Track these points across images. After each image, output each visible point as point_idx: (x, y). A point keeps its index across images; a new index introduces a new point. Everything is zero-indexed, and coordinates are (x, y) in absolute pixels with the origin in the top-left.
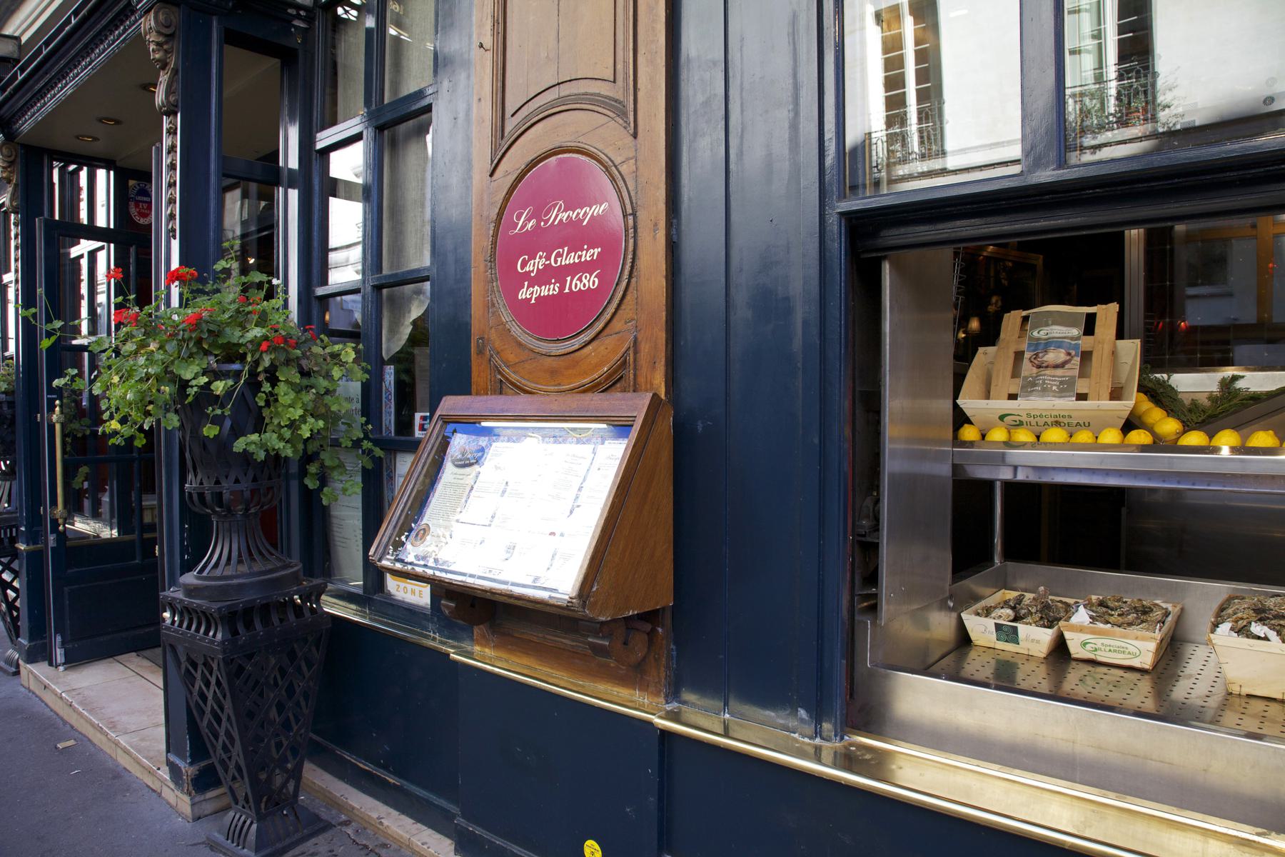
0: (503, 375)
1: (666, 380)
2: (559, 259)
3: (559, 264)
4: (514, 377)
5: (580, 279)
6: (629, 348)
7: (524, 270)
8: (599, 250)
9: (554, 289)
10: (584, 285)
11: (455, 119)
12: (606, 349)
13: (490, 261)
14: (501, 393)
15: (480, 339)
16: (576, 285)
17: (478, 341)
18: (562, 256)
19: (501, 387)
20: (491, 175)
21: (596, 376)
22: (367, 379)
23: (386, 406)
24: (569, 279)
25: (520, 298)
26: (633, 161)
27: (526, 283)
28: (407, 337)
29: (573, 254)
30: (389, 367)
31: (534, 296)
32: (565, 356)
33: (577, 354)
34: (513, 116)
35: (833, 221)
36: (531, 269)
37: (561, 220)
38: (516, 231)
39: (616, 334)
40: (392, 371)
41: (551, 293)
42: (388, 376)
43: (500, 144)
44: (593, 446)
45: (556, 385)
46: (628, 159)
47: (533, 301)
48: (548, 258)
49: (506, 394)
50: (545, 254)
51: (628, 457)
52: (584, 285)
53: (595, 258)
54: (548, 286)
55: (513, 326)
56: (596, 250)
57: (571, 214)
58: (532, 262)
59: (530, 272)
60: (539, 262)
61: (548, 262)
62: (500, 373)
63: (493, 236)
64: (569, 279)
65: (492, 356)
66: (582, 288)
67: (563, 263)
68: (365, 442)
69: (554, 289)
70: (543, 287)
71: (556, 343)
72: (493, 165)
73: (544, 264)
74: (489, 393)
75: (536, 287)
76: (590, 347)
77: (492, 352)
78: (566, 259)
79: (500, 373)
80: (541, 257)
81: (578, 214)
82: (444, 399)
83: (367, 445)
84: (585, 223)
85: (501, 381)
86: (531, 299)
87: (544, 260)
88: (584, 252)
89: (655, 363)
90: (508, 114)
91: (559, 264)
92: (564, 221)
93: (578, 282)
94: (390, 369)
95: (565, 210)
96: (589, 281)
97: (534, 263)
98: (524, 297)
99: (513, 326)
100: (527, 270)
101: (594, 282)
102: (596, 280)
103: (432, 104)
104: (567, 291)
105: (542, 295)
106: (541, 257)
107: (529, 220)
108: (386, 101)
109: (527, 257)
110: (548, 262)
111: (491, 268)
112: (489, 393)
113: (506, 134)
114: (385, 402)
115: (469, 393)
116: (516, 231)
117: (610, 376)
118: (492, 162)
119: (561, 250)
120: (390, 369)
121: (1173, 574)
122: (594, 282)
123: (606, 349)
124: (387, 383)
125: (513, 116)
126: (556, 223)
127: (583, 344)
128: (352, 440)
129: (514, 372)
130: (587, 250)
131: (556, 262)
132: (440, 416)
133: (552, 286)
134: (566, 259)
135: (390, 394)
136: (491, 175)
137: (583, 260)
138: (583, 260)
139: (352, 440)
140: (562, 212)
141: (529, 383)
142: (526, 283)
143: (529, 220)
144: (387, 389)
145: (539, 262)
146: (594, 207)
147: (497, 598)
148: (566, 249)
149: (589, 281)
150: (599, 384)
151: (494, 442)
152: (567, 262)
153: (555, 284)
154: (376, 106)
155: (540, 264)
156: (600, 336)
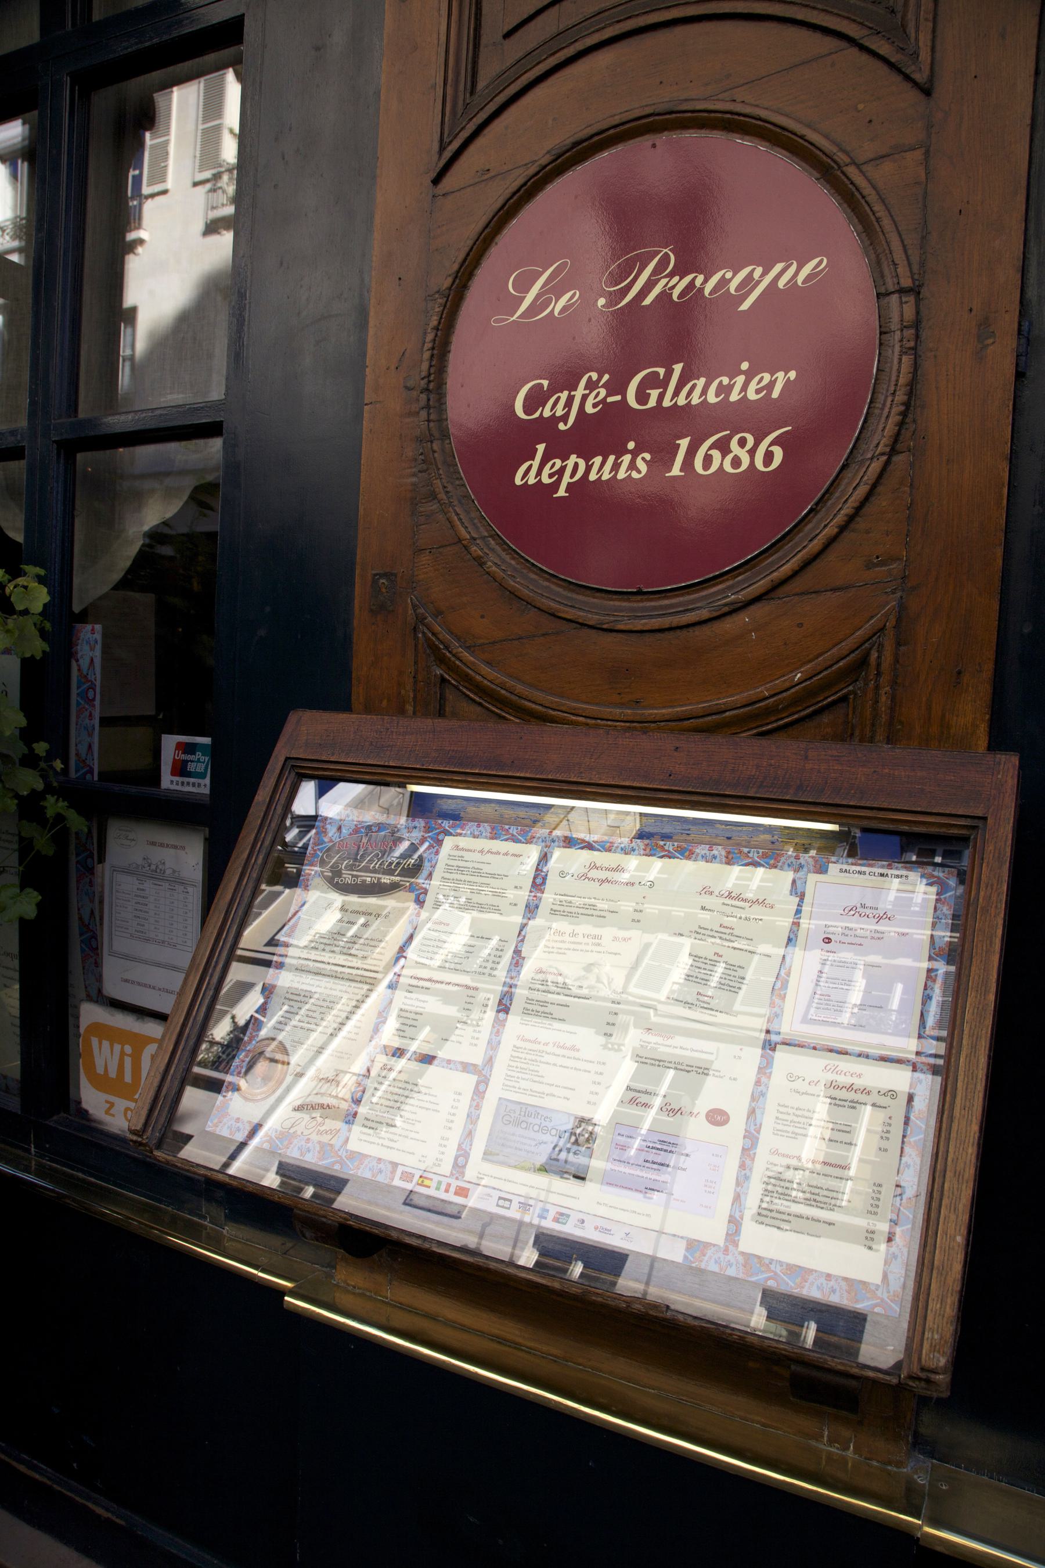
0: (451, 668)
1: (991, 720)
2: (654, 394)
3: (652, 403)
4: (488, 674)
5: (723, 447)
6: (882, 629)
7: (537, 415)
8: (792, 375)
9: (632, 466)
10: (736, 462)
11: (317, 49)
12: (800, 625)
13: (427, 390)
14: (441, 713)
15: (385, 575)
16: (708, 460)
17: (375, 582)
18: (664, 384)
19: (442, 698)
20: (436, 181)
21: (764, 691)
22: (44, 652)
23: (79, 712)
24: (684, 443)
25: (518, 481)
26: (918, 154)
27: (541, 448)
28: (128, 563)
29: (701, 382)
30: (89, 627)
31: (566, 479)
32: (659, 635)
33: (697, 631)
34: (507, 35)
35: (200, 132)
36: (560, 412)
37: (666, 295)
38: (514, 318)
39: (834, 590)
40: (98, 636)
41: (622, 475)
42: (87, 648)
43: (466, 105)
44: (790, 875)
45: (622, 705)
46: (900, 150)
47: (562, 492)
48: (618, 386)
49: (455, 715)
50: (606, 377)
51: (1000, 932)
52: (736, 462)
53: (775, 395)
54: (611, 459)
55: (493, 550)
56: (780, 375)
57: (698, 282)
58: (564, 396)
59: (554, 420)
60: (584, 398)
61: (618, 398)
62: (442, 660)
63: (437, 329)
64: (684, 443)
65: (421, 619)
66: (728, 468)
67: (667, 403)
68: (51, 799)
69: (632, 466)
70: (598, 460)
71: (628, 600)
72: (448, 154)
73: (604, 401)
74: (410, 709)
75: (573, 458)
76: (745, 618)
77: (421, 611)
78: (676, 393)
79: (442, 660)
80: (591, 386)
81: (724, 282)
82: (293, 717)
83: (53, 806)
84: (745, 306)
85: (443, 680)
86: (556, 486)
87: (603, 392)
88: (740, 380)
89: (959, 673)
90: (491, 33)
91: (652, 403)
92: (675, 297)
93: (716, 454)
94: (93, 631)
95: (680, 271)
96: (752, 452)
97: (570, 401)
98: (532, 480)
99: (493, 550)
100: (547, 413)
101: (769, 457)
102: (778, 453)
103: (243, 15)
104: (676, 471)
105: (593, 477)
106: (591, 386)
107: (554, 289)
108: (96, 17)
109: (546, 383)
110: (618, 398)
111: (428, 407)
112: (410, 709)
113: (481, 85)
114: (78, 703)
115: (345, 706)
116: (514, 318)
117: (811, 693)
118: (442, 148)
119: (662, 371)
120: (93, 631)
121: (736, 1477)
122: (769, 457)
123: (800, 625)
124: (84, 663)
125: (507, 35)
126: (648, 301)
127: (726, 609)
128: (17, 796)
129: (489, 663)
130: (749, 376)
131: (643, 398)
132: (287, 759)
133: (627, 459)
134: (676, 393)
135: (93, 687)
136: (436, 181)
137: (734, 397)
138: (734, 397)
139: (17, 796)
140: (671, 275)
141: (538, 695)
142: (541, 448)
143: (554, 289)
144: (84, 677)
145: (584, 398)
146: (779, 267)
147: (408, 1240)
148: (678, 368)
149: (752, 452)
150: (769, 711)
151: (447, 833)
152: (681, 401)
153: (635, 454)
154: (74, 25)
155: (590, 401)
156: (780, 592)
